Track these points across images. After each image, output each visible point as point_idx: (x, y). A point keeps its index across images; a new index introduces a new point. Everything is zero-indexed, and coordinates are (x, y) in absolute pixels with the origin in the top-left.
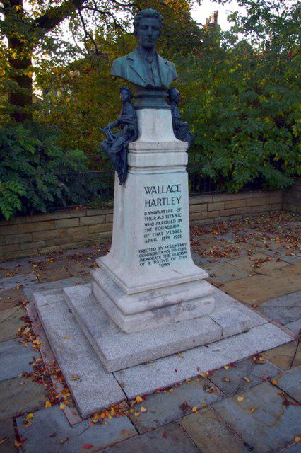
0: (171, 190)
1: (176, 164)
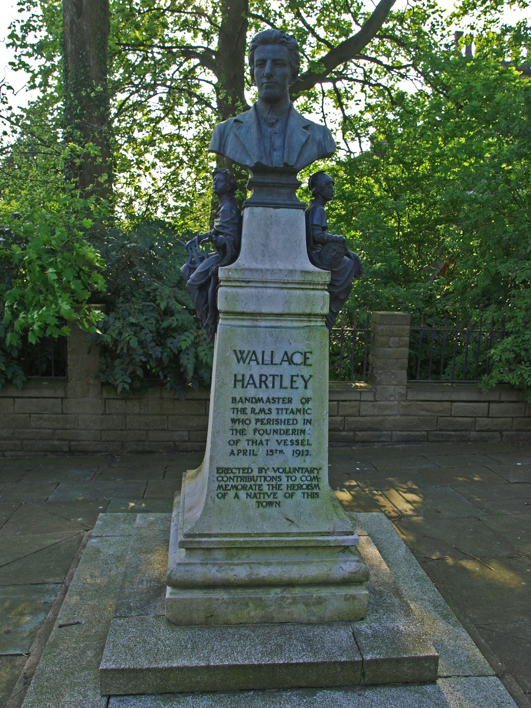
0: (290, 361)
1: (297, 311)
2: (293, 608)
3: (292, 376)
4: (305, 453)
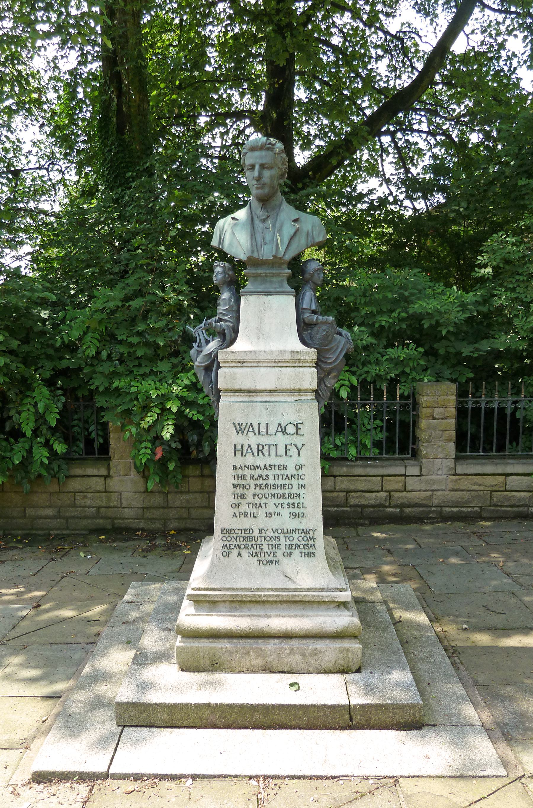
0: (284, 432)
2: (291, 658)
3: (286, 446)
4: (301, 515)
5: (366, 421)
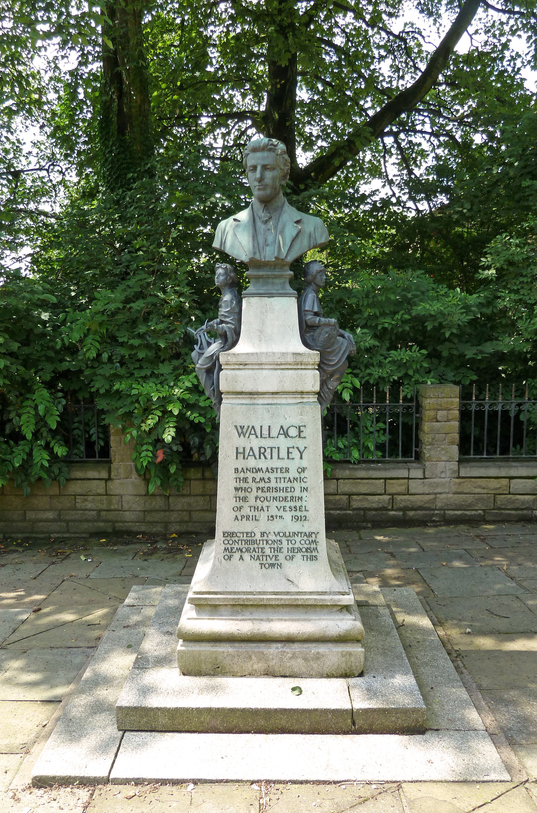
0: (286, 435)
2: (293, 662)
3: (288, 448)
4: (303, 518)
5: (369, 424)
